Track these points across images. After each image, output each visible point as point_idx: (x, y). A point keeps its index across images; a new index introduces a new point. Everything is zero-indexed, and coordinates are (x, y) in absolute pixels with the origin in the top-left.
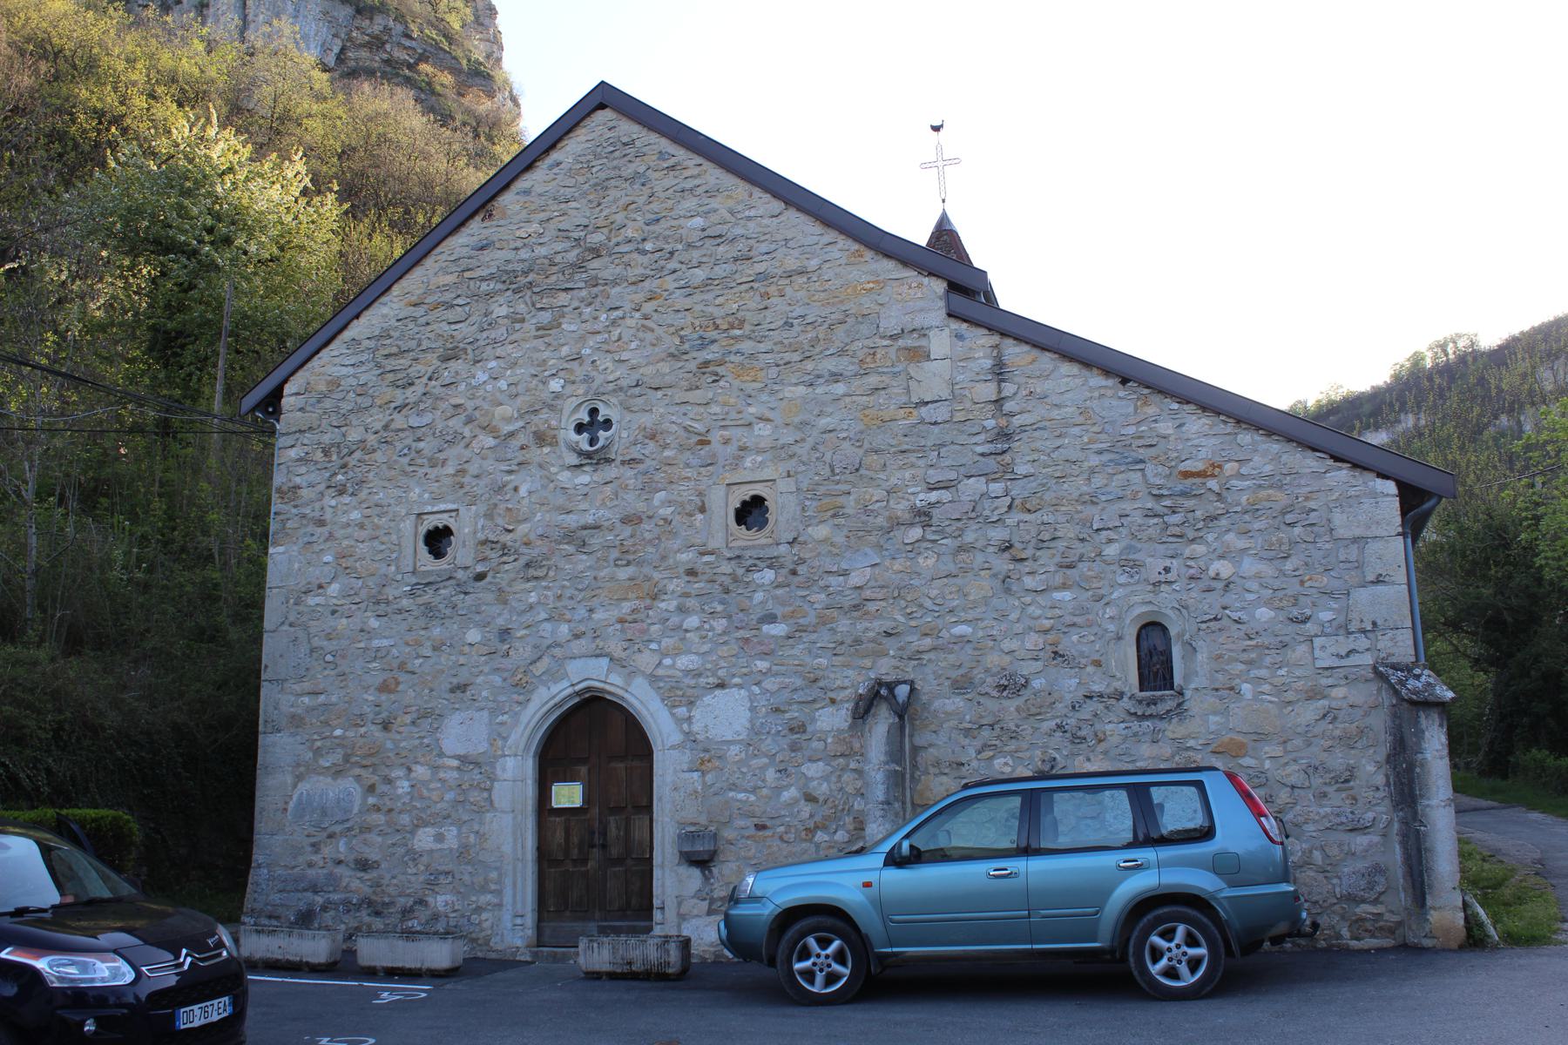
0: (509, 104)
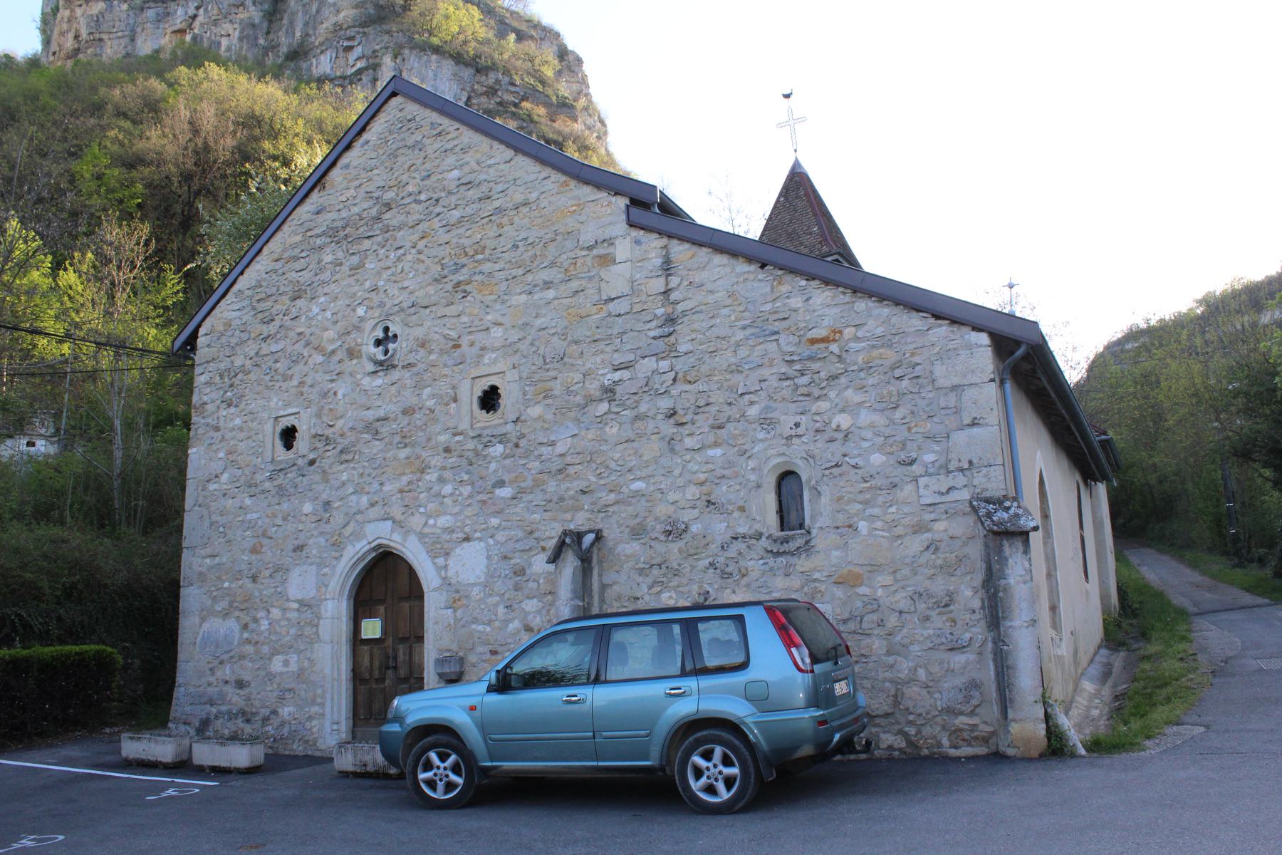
0: (599, 125)
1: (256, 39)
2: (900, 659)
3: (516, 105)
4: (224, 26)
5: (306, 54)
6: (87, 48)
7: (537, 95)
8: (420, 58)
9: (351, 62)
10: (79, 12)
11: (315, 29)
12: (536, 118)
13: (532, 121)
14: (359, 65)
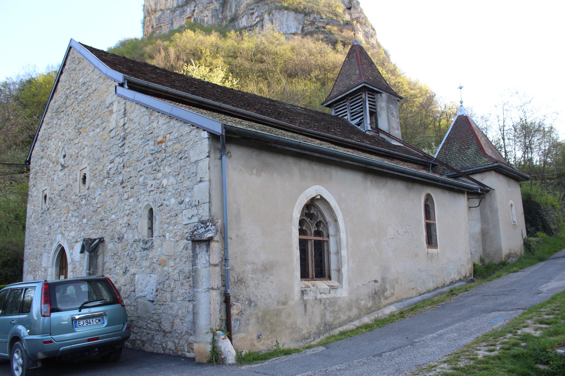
0: (372, 31)
1: (218, 15)
2: (175, 304)
3: (324, 28)
4: (205, 12)
5: (237, 18)
6: (156, 31)
7: (334, 21)
8: (279, 13)
9: (254, 19)
10: (153, 17)
11: (240, 7)
12: (333, 32)
13: (331, 34)
14: (257, 20)
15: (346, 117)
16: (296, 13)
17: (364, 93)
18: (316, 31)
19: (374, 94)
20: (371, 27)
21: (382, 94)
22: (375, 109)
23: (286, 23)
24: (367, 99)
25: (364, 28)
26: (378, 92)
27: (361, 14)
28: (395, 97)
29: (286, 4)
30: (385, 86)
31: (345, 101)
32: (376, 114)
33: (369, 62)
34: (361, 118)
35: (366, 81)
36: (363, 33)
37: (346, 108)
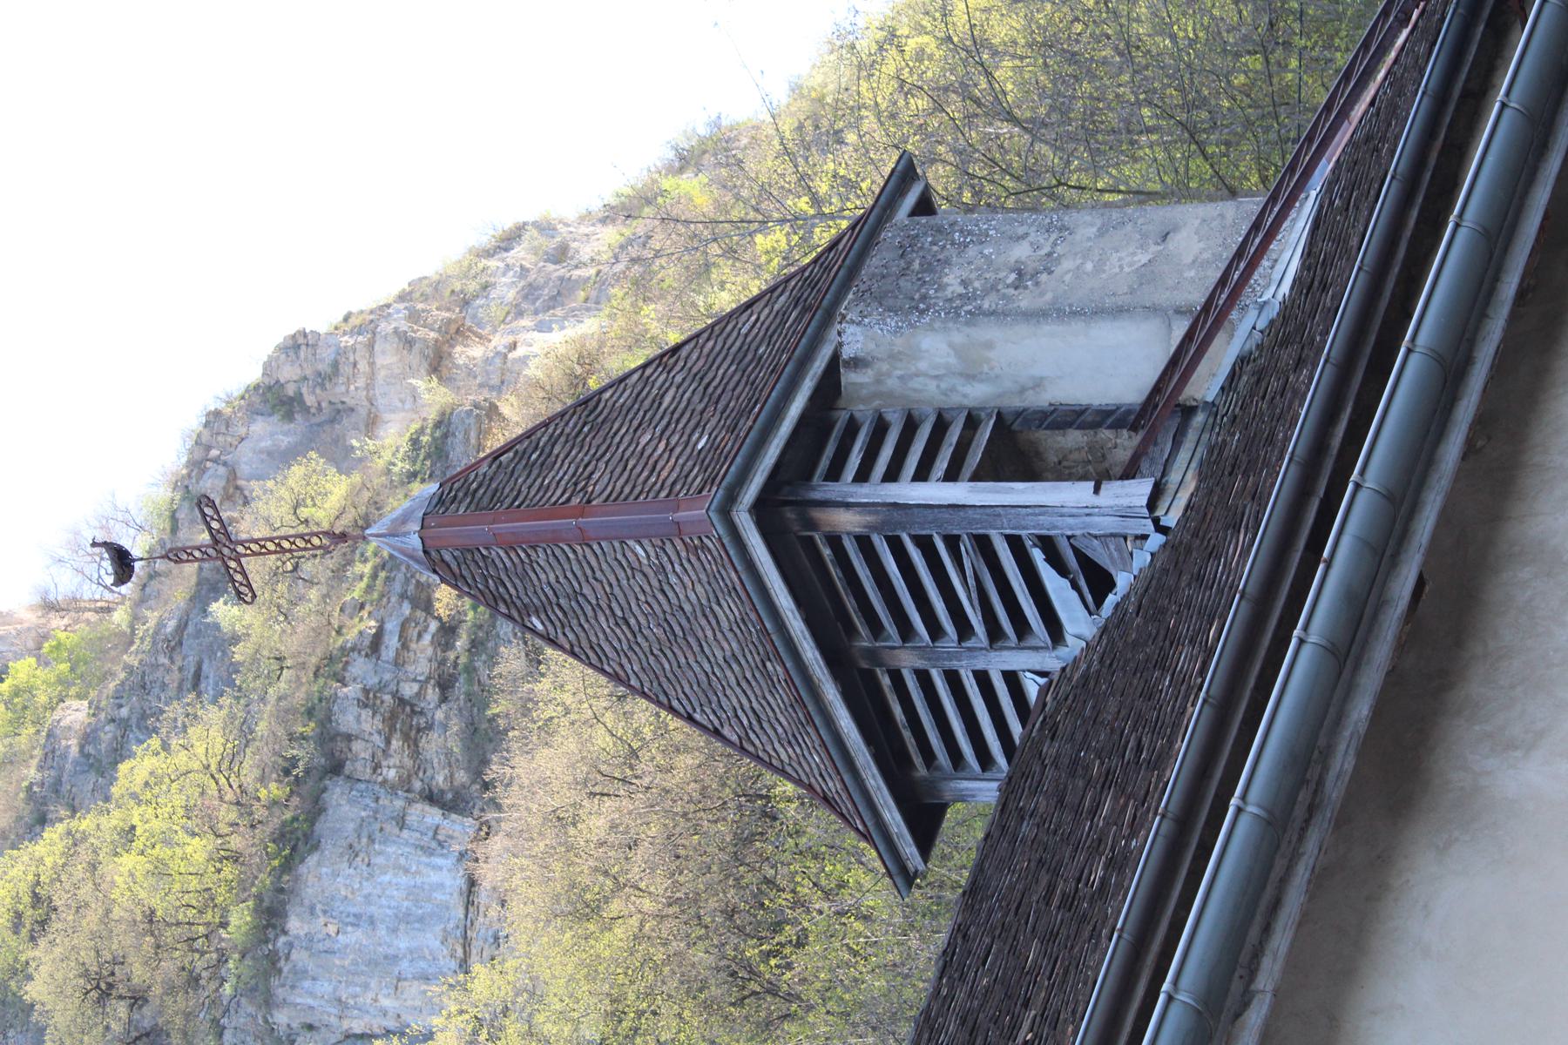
0: (520, 254)
3: (448, 631)
8: (300, 974)
15: (1032, 688)
16: (316, 847)
17: (819, 514)
18: (469, 697)
19: (842, 418)
20: (488, 253)
21: (847, 353)
22: (972, 422)
23: (382, 931)
24: (878, 491)
25: (496, 312)
26: (829, 386)
27: (385, 327)
28: (887, 234)
29: (241, 918)
30: (783, 314)
31: (886, 681)
32: (1019, 414)
33: (574, 440)
34: (1038, 556)
35: (716, 494)
36: (526, 322)
37: (953, 678)
